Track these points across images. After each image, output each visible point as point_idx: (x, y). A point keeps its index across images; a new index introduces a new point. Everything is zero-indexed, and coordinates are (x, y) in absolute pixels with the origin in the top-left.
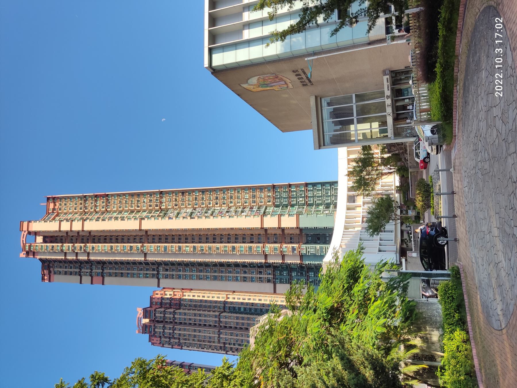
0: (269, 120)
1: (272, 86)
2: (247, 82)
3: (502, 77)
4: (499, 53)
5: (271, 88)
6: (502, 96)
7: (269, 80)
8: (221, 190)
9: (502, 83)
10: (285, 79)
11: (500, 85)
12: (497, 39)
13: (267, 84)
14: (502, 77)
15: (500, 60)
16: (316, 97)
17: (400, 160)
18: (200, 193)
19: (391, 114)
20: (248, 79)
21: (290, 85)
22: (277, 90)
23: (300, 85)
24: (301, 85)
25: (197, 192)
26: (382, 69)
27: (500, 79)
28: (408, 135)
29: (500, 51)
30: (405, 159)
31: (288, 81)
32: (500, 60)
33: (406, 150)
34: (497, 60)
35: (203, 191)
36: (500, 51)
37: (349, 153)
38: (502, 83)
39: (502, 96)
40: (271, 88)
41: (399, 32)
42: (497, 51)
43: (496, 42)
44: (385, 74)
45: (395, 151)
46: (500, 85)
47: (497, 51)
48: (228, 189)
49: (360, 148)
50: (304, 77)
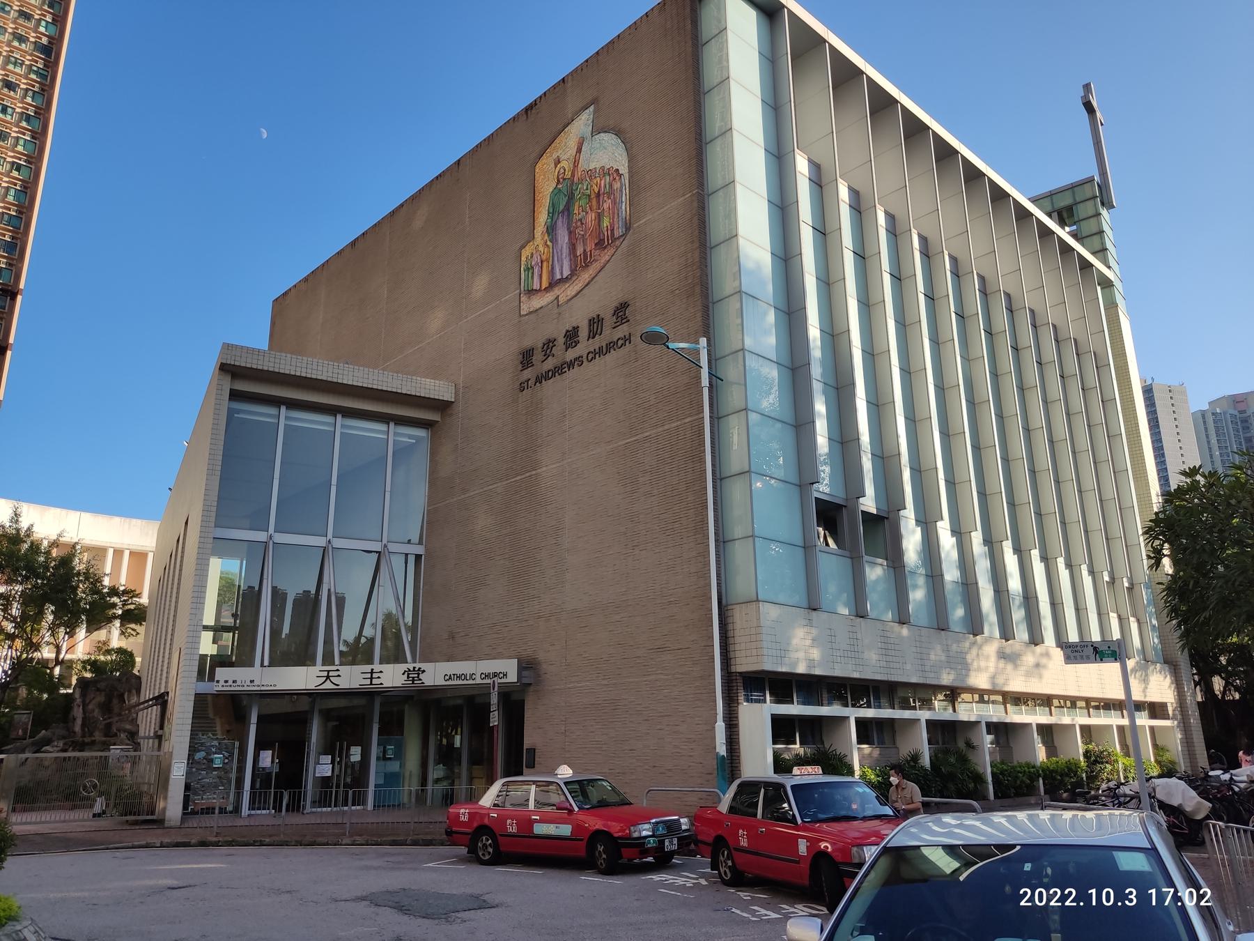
0: (353, 244)
1: (551, 230)
2: (597, 130)
3: (1067, 903)
4: (1126, 897)
5: (540, 229)
6: (1022, 903)
7: (591, 217)
8: (42, 113)
9: (1052, 903)
10: (585, 276)
11: (1049, 900)
12: (1159, 893)
13: (568, 208)
14: (1067, 903)
15: (1108, 900)
16: (443, 406)
17: (40, 721)
18: (45, 40)
19: (328, 685)
20: (618, 133)
21: (537, 302)
22: (526, 253)
23: (534, 339)
24: (527, 343)
25: (52, 31)
26: (541, 656)
27: (1063, 898)
28: (199, 755)
29: (1131, 901)
30: (48, 742)
31: (571, 289)
32: (1108, 900)
33: (81, 747)
34: (1108, 893)
35: (49, 51)
36: (1131, 901)
37: (139, 557)
38: (1052, 903)
39: (1022, 903)
40: (540, 229)
41: (341, 653)
42: (1131, 893)
43: (1153, 891)
44: (527, 666)
45: (85, 705)
46: (1049, 900)
47: (1131, 893)
48: (39, 136)
49: (123, 581)
50: (571, 355)
